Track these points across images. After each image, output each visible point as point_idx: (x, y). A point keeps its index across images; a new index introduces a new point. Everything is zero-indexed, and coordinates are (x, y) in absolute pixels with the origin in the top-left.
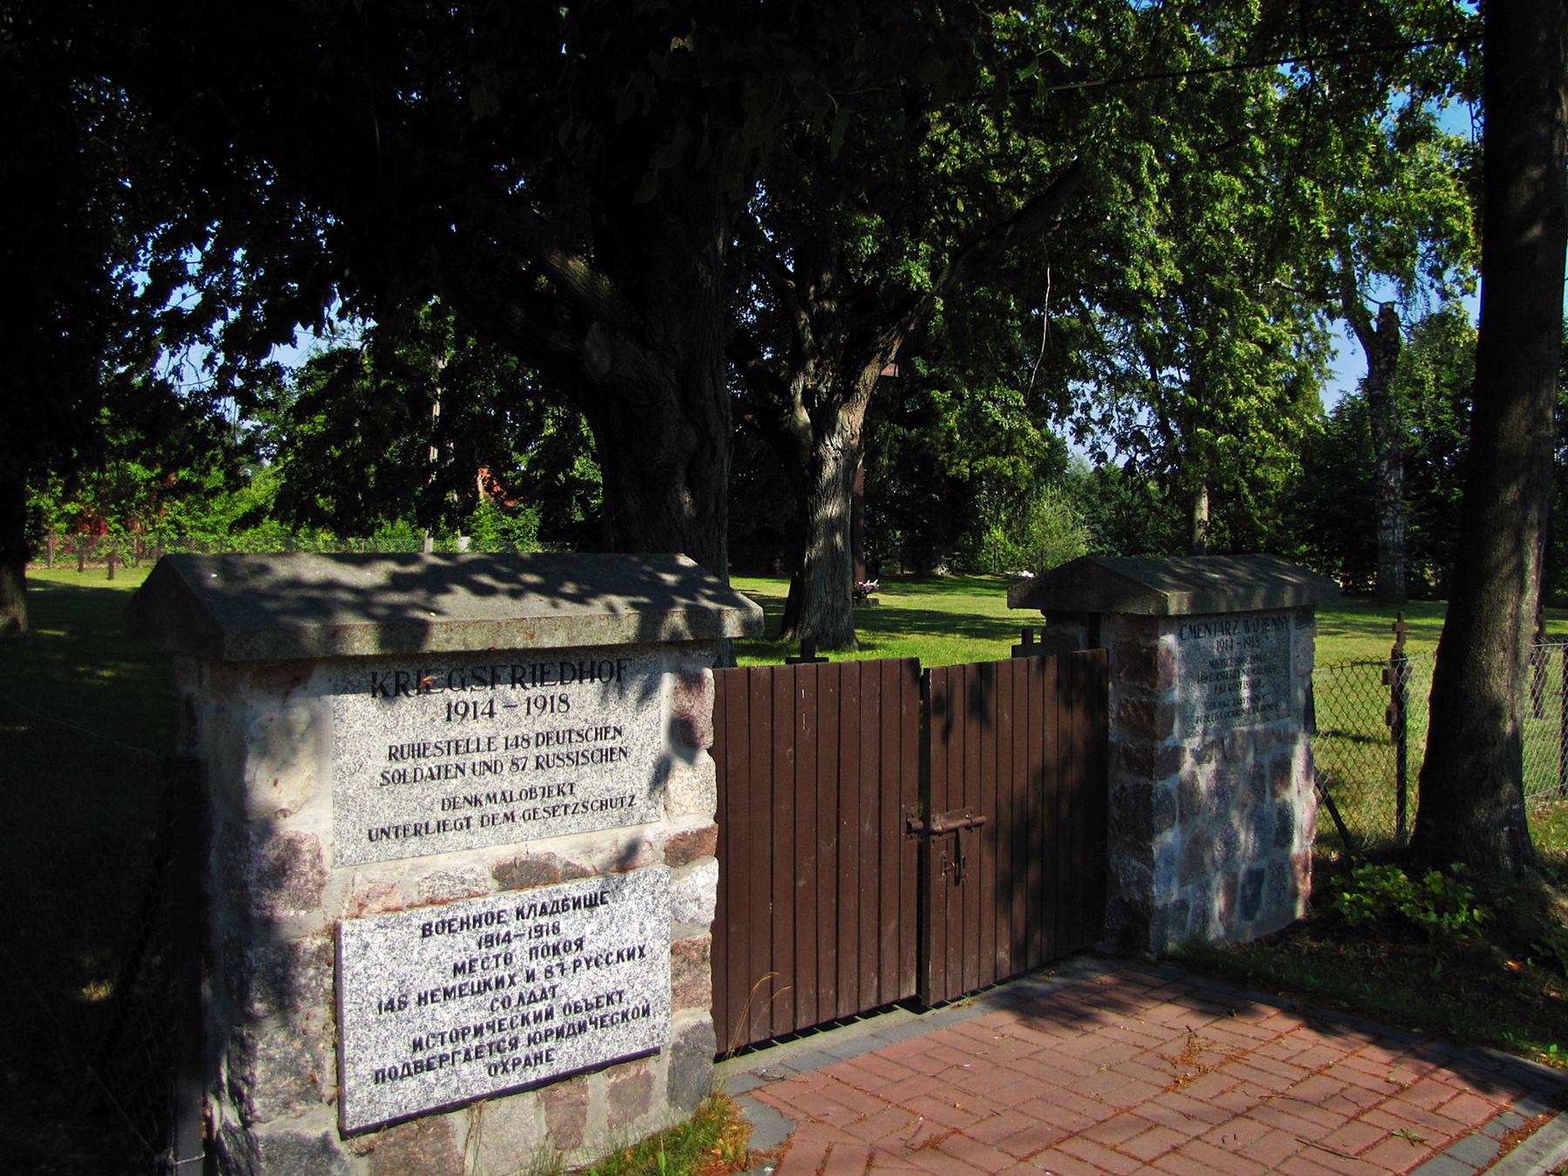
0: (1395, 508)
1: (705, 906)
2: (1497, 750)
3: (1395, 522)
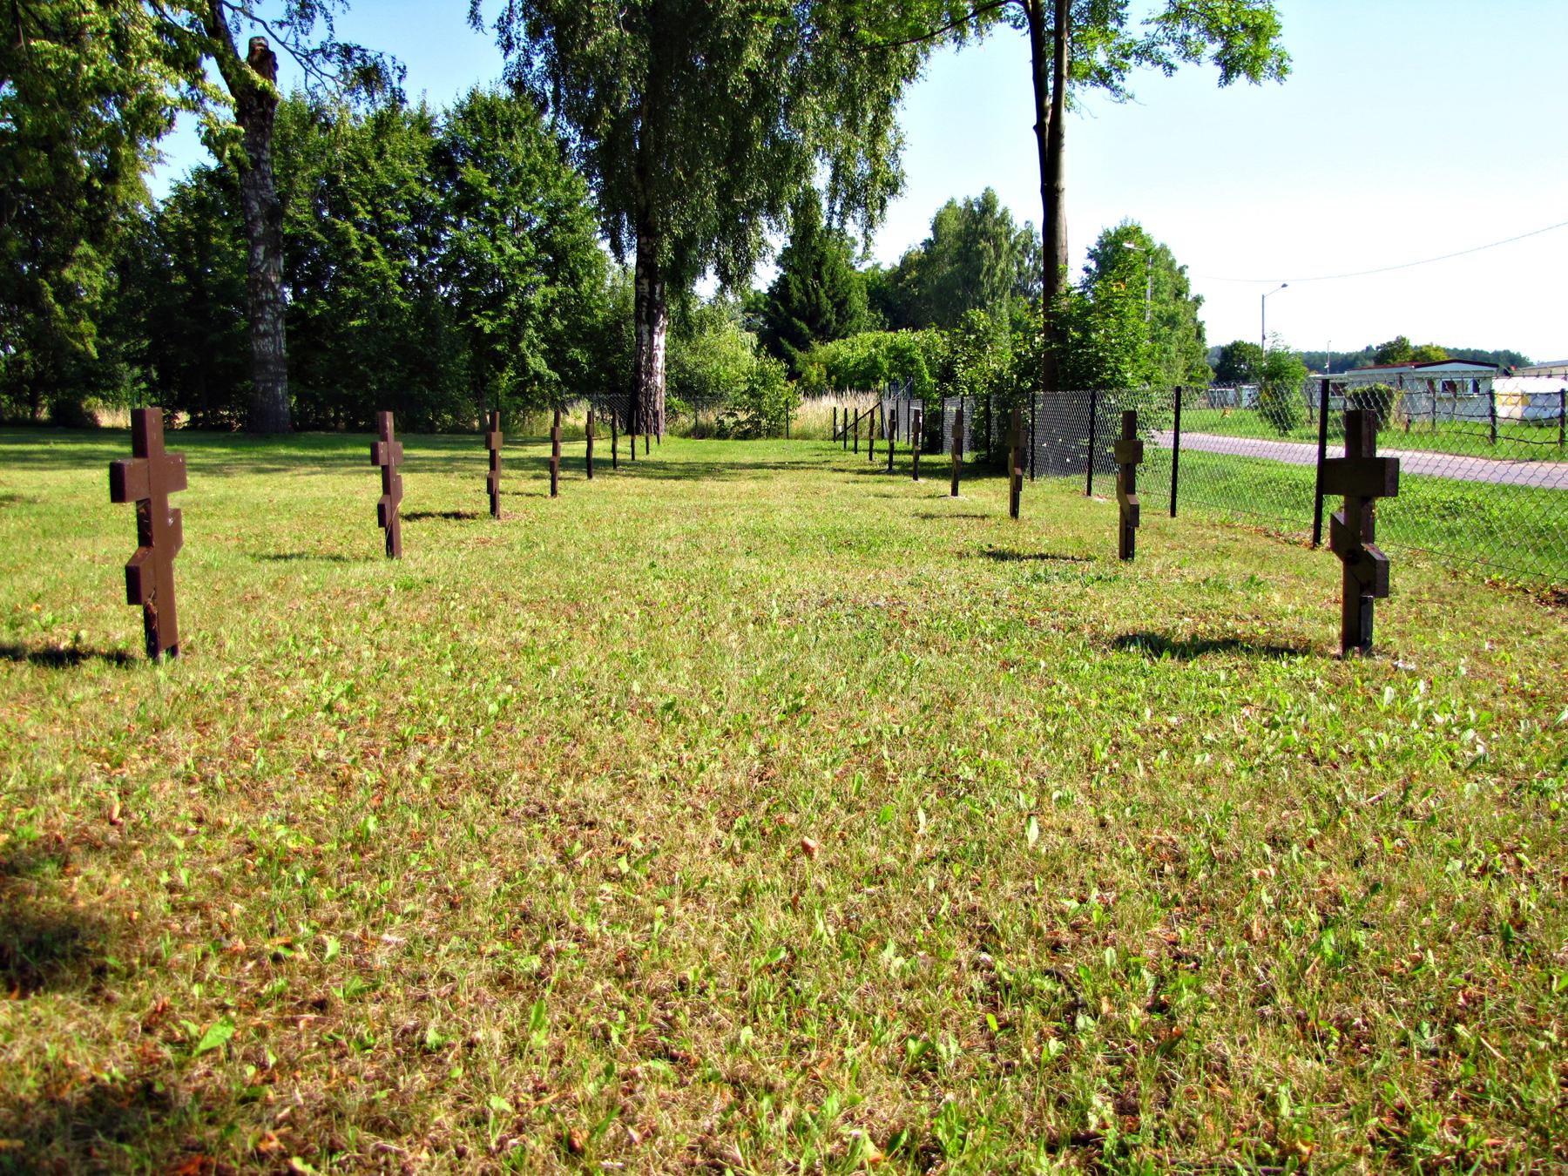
0: (275, 309)
3: (275, 327)
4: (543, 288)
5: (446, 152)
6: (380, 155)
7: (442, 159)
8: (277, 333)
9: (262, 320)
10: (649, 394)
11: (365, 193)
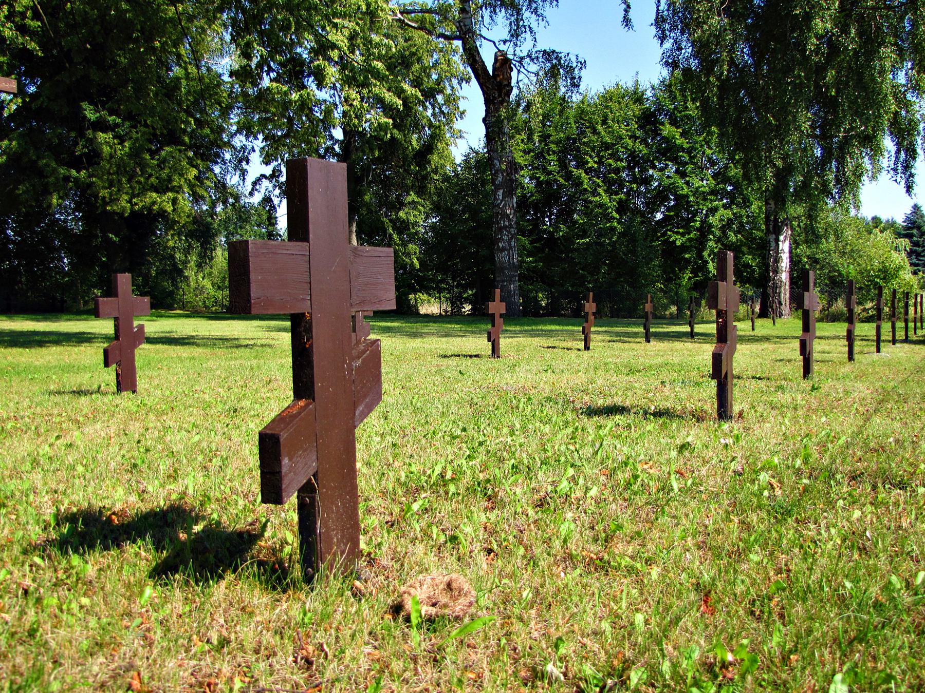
0: (510, 232)
1: (105, 562)
2: (71, 553)
3: (510, 244)
4: (722, 211)
5: (653, 115)
6: (604, 122)
7: (649, 120)
8: (511, 248)
9: (501, 239)
10: (776, 287)
11: (593, 150)
